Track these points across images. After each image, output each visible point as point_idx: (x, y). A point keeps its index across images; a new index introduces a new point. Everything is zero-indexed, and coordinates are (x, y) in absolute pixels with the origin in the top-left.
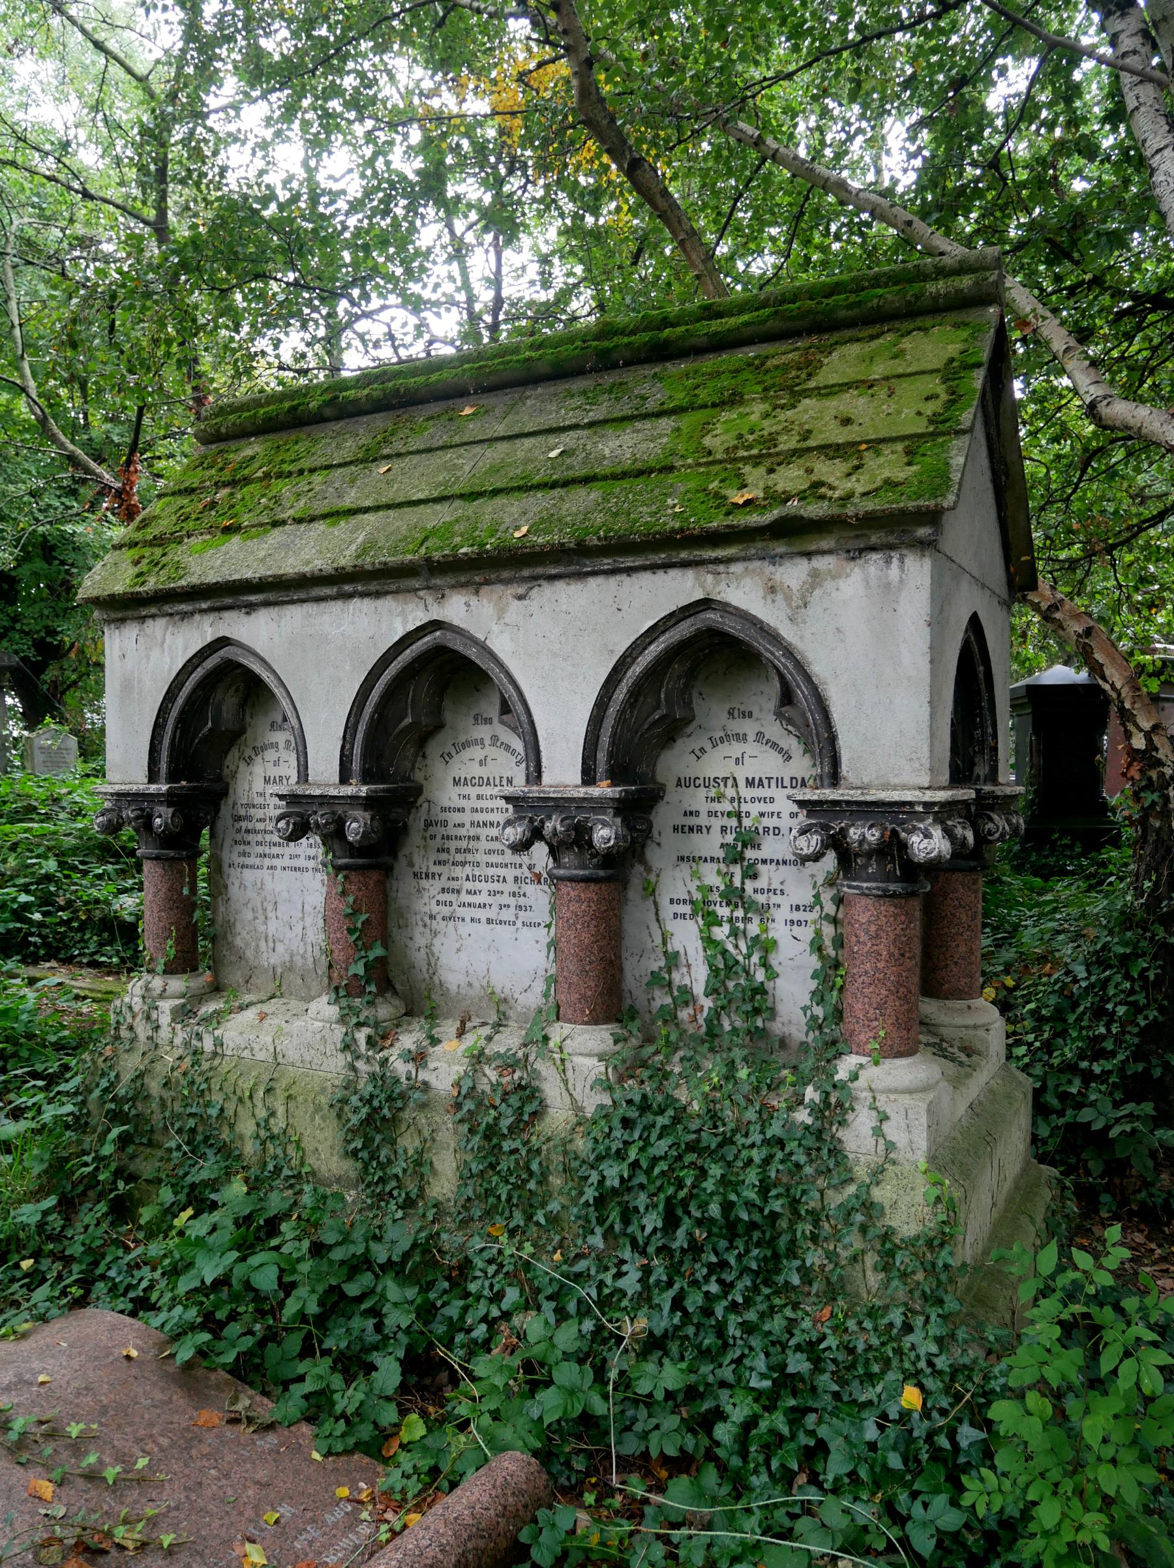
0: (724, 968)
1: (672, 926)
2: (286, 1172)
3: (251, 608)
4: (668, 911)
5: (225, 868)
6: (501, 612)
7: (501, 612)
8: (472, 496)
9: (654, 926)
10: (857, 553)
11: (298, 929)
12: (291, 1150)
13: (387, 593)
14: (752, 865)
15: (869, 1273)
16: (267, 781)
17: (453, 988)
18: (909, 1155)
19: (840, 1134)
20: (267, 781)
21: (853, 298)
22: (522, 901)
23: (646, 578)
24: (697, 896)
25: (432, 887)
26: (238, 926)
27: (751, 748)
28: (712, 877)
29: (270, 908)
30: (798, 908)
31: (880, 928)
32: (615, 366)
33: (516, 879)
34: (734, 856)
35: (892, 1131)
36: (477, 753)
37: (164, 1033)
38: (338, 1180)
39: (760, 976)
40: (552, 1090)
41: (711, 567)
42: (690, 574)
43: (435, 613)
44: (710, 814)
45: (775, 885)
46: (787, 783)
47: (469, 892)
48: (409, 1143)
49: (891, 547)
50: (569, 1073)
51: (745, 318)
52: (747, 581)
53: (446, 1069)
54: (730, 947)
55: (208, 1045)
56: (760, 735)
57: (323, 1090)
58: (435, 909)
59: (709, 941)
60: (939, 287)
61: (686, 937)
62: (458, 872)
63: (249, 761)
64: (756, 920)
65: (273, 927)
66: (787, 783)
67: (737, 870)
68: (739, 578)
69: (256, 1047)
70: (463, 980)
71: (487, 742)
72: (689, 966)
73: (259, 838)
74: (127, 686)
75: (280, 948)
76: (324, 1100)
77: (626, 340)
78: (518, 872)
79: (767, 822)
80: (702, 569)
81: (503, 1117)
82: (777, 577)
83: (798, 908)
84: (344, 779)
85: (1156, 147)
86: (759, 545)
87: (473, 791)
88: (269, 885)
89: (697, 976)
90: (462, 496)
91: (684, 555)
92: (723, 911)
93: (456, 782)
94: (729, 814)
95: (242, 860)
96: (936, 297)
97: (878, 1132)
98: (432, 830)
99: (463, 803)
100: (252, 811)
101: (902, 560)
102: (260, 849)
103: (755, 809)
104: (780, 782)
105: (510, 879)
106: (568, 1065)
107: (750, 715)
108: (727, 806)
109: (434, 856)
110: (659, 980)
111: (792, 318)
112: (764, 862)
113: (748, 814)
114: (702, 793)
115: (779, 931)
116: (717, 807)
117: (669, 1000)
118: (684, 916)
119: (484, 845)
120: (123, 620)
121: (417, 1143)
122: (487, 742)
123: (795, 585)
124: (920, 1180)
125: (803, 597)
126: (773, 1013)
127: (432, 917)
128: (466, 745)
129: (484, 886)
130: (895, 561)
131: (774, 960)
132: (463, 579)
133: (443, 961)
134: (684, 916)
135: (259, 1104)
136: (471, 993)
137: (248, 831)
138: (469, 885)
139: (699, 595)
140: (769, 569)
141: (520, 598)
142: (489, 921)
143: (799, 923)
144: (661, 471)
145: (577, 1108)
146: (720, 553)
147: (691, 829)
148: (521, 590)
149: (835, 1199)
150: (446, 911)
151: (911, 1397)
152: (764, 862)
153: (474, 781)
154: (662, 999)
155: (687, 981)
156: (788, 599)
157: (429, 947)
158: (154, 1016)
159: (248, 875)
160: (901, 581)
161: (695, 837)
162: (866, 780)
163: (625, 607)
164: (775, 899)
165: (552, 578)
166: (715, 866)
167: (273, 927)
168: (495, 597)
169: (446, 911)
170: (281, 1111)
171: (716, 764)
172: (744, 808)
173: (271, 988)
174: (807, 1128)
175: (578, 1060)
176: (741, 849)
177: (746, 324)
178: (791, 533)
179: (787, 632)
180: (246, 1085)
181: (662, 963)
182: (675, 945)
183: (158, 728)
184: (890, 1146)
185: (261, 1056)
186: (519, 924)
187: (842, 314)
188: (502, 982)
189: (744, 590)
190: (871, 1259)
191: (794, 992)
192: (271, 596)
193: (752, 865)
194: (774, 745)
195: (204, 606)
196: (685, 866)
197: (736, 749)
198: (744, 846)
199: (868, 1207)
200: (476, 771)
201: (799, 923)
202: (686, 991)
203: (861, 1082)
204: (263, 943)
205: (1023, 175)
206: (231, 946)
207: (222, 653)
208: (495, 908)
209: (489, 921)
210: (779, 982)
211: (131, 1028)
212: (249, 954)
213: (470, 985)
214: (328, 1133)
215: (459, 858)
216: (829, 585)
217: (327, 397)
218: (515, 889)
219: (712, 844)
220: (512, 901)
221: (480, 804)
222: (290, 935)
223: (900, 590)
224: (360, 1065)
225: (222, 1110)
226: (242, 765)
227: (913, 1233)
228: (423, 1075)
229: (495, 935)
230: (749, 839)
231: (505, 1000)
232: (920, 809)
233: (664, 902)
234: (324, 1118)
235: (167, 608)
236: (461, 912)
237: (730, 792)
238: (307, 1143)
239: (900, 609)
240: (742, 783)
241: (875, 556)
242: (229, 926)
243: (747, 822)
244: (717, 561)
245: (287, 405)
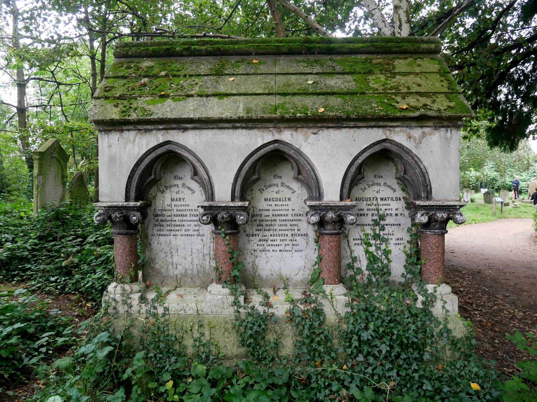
0: (372, 259)
1: (353, 248)
2: (211, 357)
3: (185, 129)
4: (352, 243)
5: (150, 236)
6: (306, 139)
7: (306, 139)
8: (285, 94)
9: (347, 248)
10: (436, 128)
11: (189, 259)
12: (213, 348)
13: (256, 128)
14: (383, 226)
15: (447, 351)
16: (172, 200)
17: (265, 277)
18: (453, 313)
19: (431, 310)
20: (172, 200)
21: (398, 45)
22: (295, 243)
23: (364, 130)
24: (363, 237)
25: (255, 240)
26: (157, 260)
27: (382, 188)
28: (368, 230)
29: (174, 251)
30: (398, 239)
31: (439, 244)
32: (313, 53)
33: (292, 235)
34: (376, 223)
35: (448, 307)
36: (275, 189)
37: (135, 308)
38: (237, 356)
39: (385, 261)
40: (327, 309)
41: (388, 128)
42: (381, 130)
43: (277, 137)
44: (368, 210)
45: (391, 232)
46: (394, 199)
47: (272, 241)
48: (271, 337)
49: (448, 127)
50: (334, 303)
51: (361, 45)
52: (401, 134)
53: (280, 307)
54: (375, 254)
55: (160, 310)
56: (385, 183)
57: (227, 322)
58: (256, 247)
59: (367, 252)
60: (424, 46)
61: (359, 251)
62: (267, 233)
63: (163, 192)
64: (384, 244)
65: (175, 259)
66: (394, 199)
67: (377, 228)
68: (398, 133)
69: (187, 309)
70: (269, 273)
71: (279, 185)
72: (360, 261)
73: (169, 223)
74: (112, 159)
75: (180, 268)
76: (229, 326)
77: (318, 45)
78: (293, 232)
79: (388, 212)
80: (386, 128)
81: (308, 322)
82: (411, 133)
83: (398, 239)
84: (233, 200)
85: (373, 8)
86: (408, 123)
87: (273, 203)
88: (174, 242)
89: (363, 263)
90: (279, 94)
91: (381, 124)
92: (373, 242)
93: (266, 200)
94: (375, 210)
95: (159, 233)
96: (423, 49)
97: (443, 307)
98: (254, 218)
99: (269, 208)
100: (165, 213)
101: (451, 131)
102: (169, 228)
103: (383, 208)
104: (392, 199)
105: (290, 235)
106: (334, 299)
107: (382, 177)
108: (374, 207)
109: (255, 228)
110: (350, 266)
111: (377, 48)
112: (387, 225)
113: (381, 210)
114: (365, 202)
115: (392, 247)
116: (370, 207)
117: (353, 273)
118: (358, 244)
119: (278, 223)
120: (110, 131)
121: (275, 336)
122: (279, 185)
123: (417, 136)
124: (459, 320)
125: (420, 140)
126: (390, 274)
127: (254, 251)
128: (270, 186)
129: (278, 238)
130: (449, 131)
131: (390, 257)
132: (292, 125)
133: (260, 267)
134: (358, 244)
135: (196, 332)
136: (273, 277)
137: (162, 221)
138: (272, 238)
139: (384, 137)
140: (408, 130)
141: (314, 134)
142: (280, 251)
143: (399, 244)
144: (361, 94)
145: (337, 314)
146: (390, 124)
147: (361, 215)
148: (315, 131)
149: (437, 331)
150: (261, 248)
151: (475, 386)
152: (387, 225)
153: (182, 198)
154: (350, 273)
155: (359, 266)
156: (415, 141)
157: (254, 262)
158: (129, 301)
159: (162, 239)
160: (451, 137)
161: (362, 217)
162: (440, 198)
163: (357, 140)
164: (390, 237)
165: (328, 128)
166: (370, 227)
167: (175, 259)
168: (304, 133)
169: (261, 248)
170: (207, 333)
171: (370, 193)
172: (380, 207)
173: (175, 284)
174: (421, 309)
175: (338, 297)
176: (380, 220)
177: (362, 47)
178: (422, 120)
179: (414, 151)
180: (188, 326)
181: (351, 261)
182: (355, 254)
183: (130, 178)
184: (447, 311)
185: (190, 312)
186: (293, 251)
187: (394, 49)
188: (286, 272)
189: (400, 136)
190: (448, 347)
191: (398, 267)
192: (198, 125)
193: (383, 226)
194: (390, 187)
195: (161, 127)
196: (359, 227)
197: (376, 188)
198: (380, 220)
199: (449, 331)
200: (275, 196)
201: (399, 244)
202: (359, 269)
203: (438, 293)
204: (170, 266)
205: (365, 9)
206: (153, 269)
207: (166, 146)
208: (283, 246)
209: (280, 251)
210: (391, 263)
211: (115, 308)
212: (163, 271)
213: (272, 275)
214: (232, 339)
215: (267, 228)
216: (428, 137)
217: (186, 47)
218: (292, 238)
219: (368, 220)
220: (290, 243)
221: (276, 208)
222: (184, 262)
223: (450, 140)
224: (242, 310)
225: (175, 337)
226: (159, 194)
227: (461, 336)
228: (271, 311)
229: (286, 257)
230: (382, 217)
231: (287, 279)
232: (458, 207)
233: (351, 240)
234: (229, 333)
235: (139, 127)
236: (268, 248)
237: (375, 202)
238: (221, 344)
239: (451, 146)
240: (379, 199)
241: (443, 129)
242: (152, 260)
243: (381, 212)
244: (391, 127)
245: (165, 47)
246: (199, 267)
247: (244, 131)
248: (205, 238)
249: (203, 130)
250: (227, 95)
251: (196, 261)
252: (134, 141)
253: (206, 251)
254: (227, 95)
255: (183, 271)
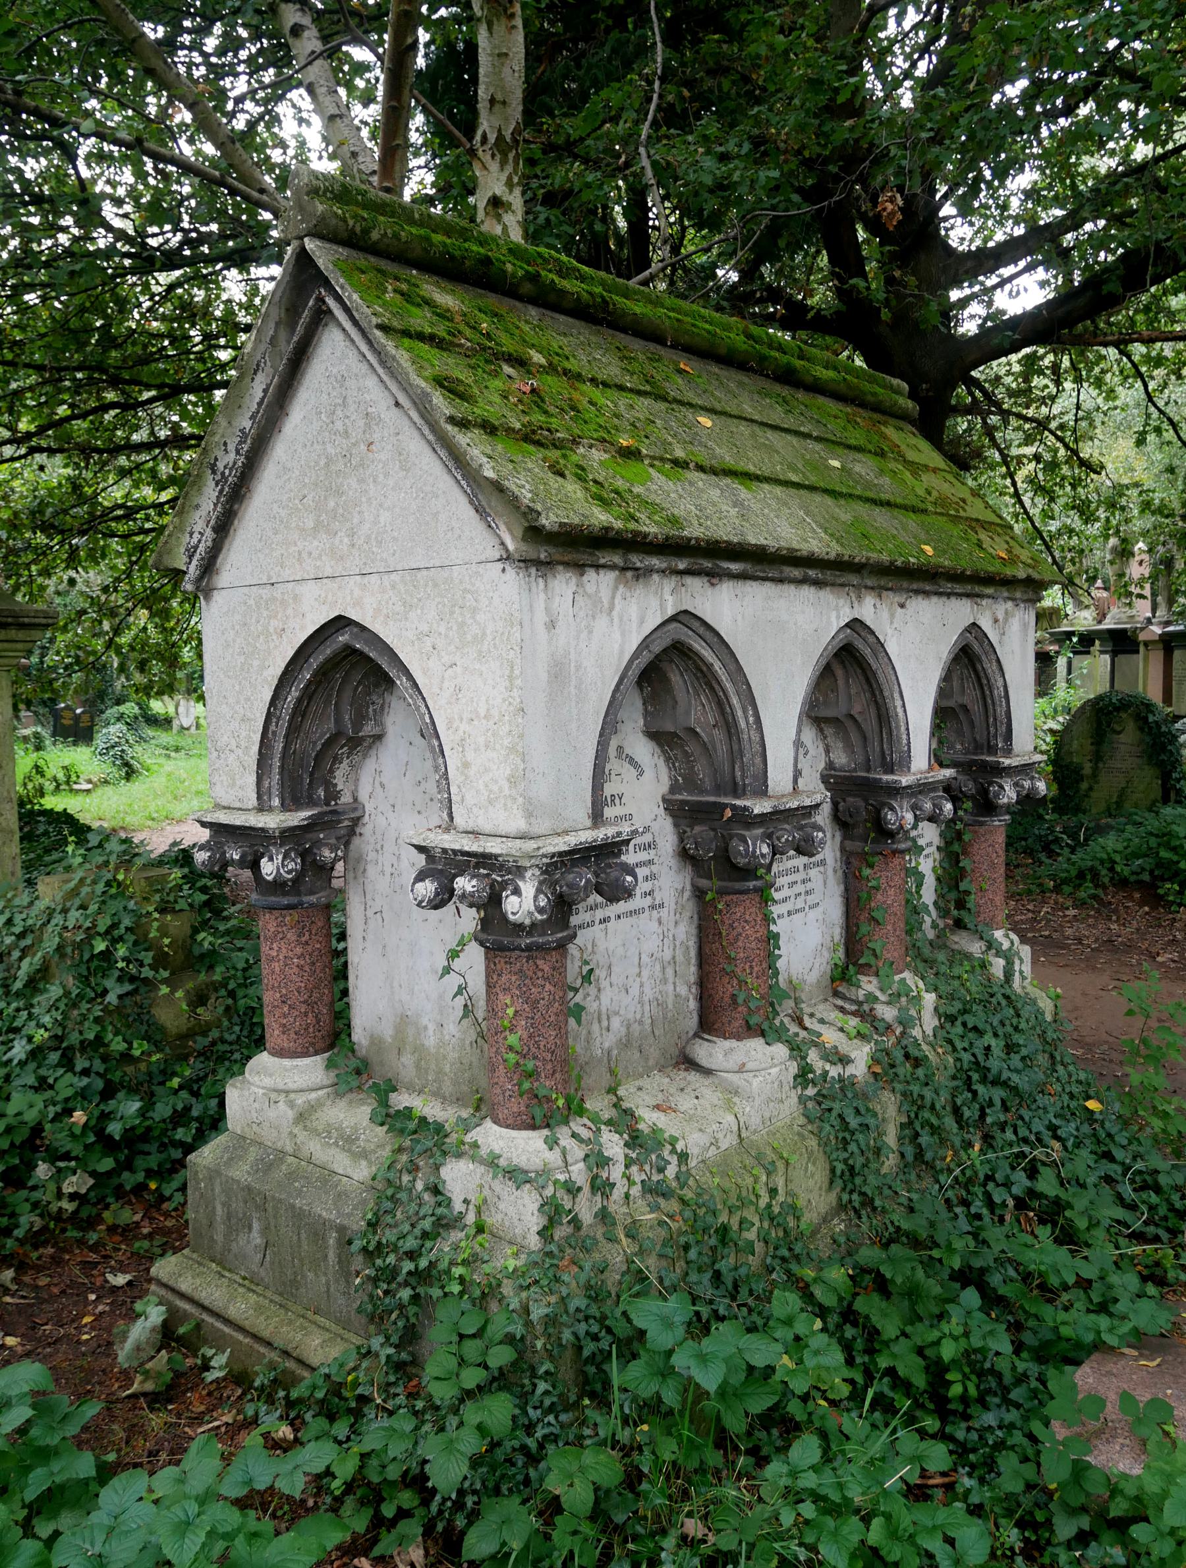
11: (635, 991)
75: (616, 1023)
148: (898, 598)
246: (654, 1010)
247: (807, 592)
248: (664, 913)
249: (749, 583)
250: (758, 478)
251: (649, 993)
252: (612, 608)
253: (667, 955)
254: (758, 478)
255: (624, 1030)
